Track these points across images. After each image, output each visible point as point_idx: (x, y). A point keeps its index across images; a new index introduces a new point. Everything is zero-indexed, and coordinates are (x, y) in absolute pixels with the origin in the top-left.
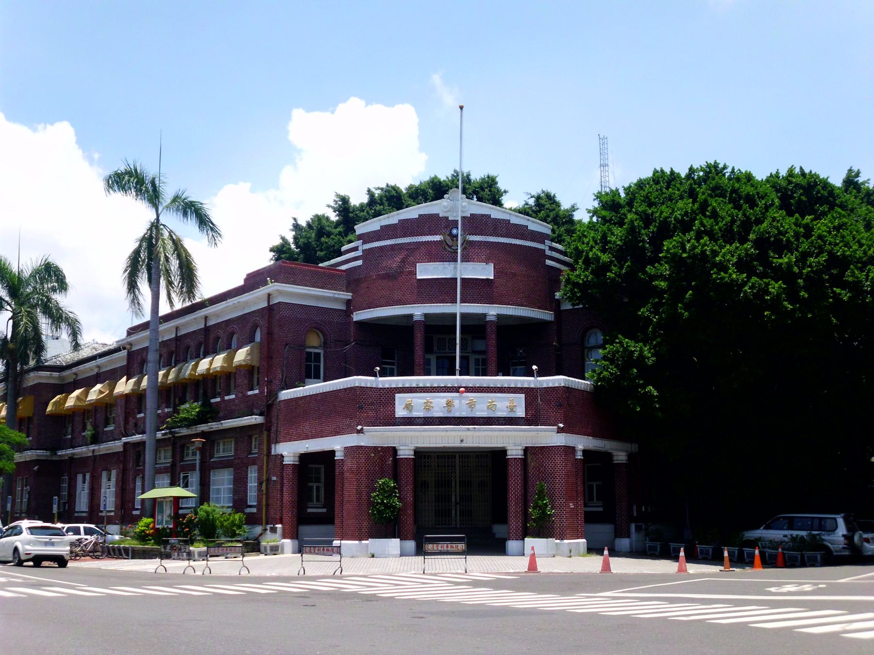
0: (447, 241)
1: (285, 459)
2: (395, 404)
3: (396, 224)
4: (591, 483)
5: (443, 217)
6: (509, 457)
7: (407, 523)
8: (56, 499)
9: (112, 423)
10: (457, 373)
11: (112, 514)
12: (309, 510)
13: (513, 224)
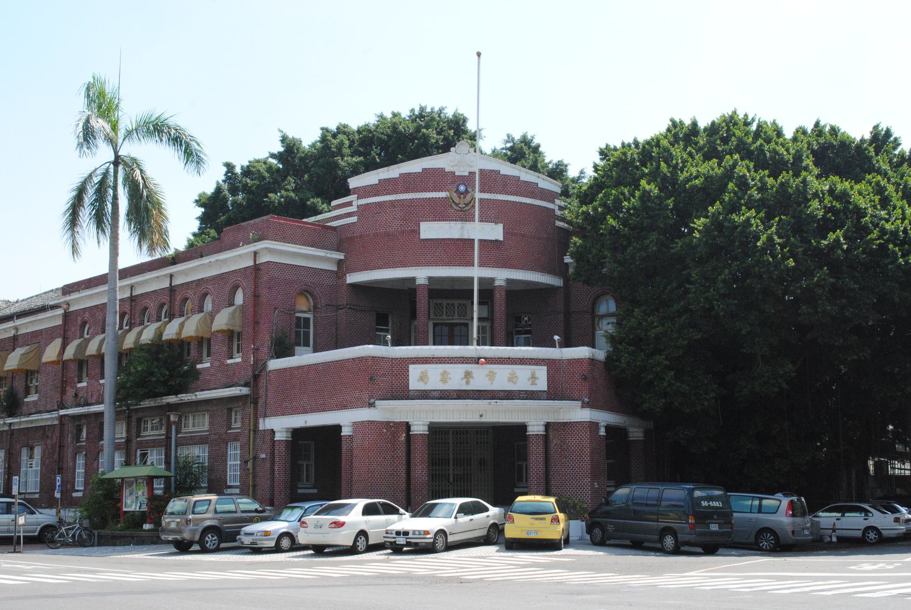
1: (277, 435)
2: (408, 375)
3: (396, 178)
4: (520, 463)
5: (449, 172)
6: (530, 433)
8: (16, 479)
9: (34, 393)
11: (37, 496)
12: (300, 491)
13: (522, 181)
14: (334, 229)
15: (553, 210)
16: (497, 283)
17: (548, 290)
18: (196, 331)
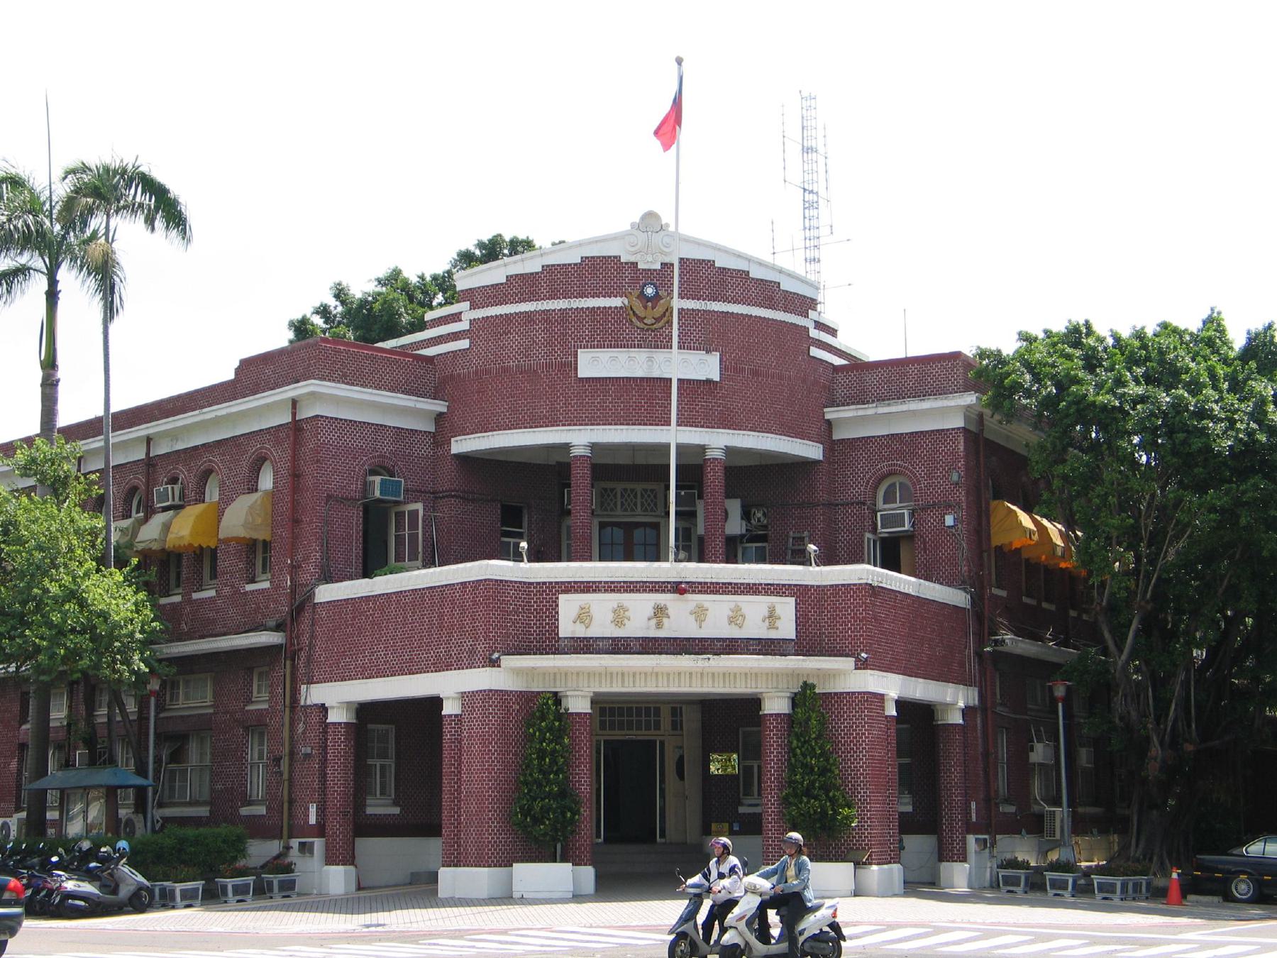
0: (634, 308)
10: (672, 556)
12: (742, 810)
14: (430, 360)
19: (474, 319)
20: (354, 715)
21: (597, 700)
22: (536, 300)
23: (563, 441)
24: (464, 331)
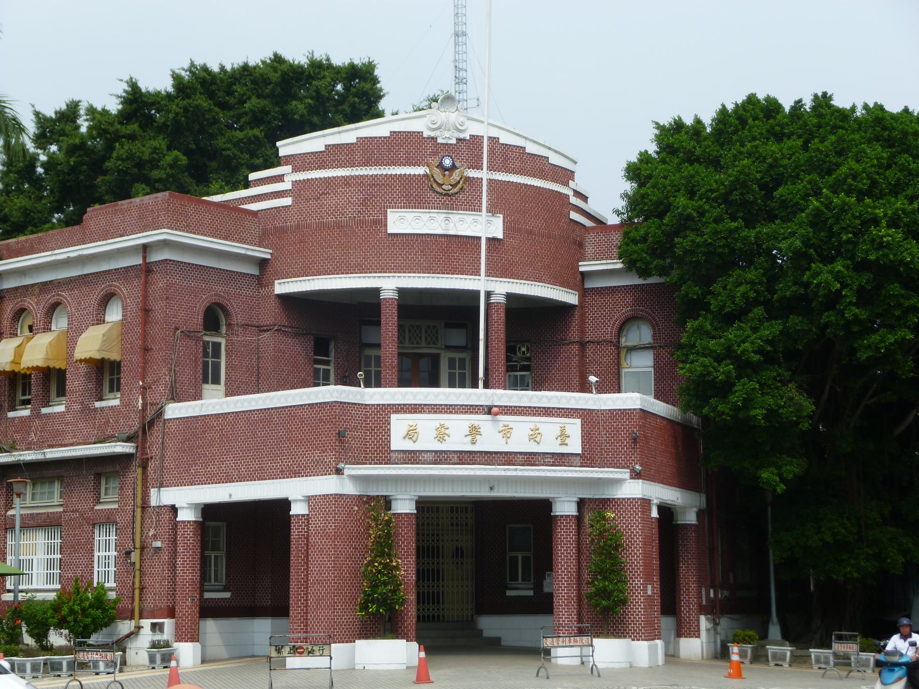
2: (389, 430)
3: (352, 144)
4: (514, 554)
7: (408, 615)
12: (509, 593)
14: (255, 214)
15: (567, 196)
16: (383, 295)
17: (563, 309)
18: (47, 359)
19: (296, 181)
20: (200, 515)
21: (423, 505)
22: (351, 166)
23: (374, 286)
24: (286, 191)
